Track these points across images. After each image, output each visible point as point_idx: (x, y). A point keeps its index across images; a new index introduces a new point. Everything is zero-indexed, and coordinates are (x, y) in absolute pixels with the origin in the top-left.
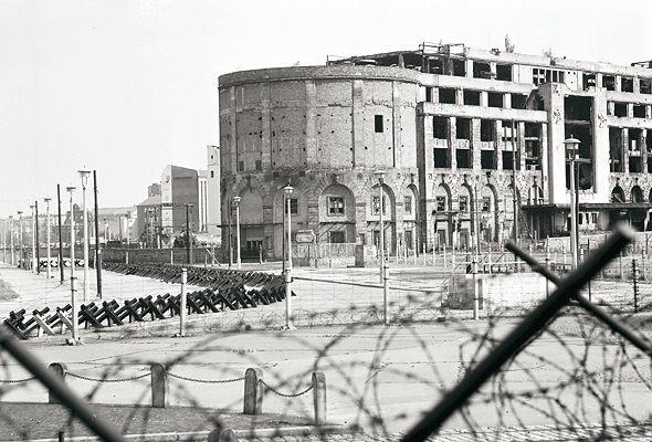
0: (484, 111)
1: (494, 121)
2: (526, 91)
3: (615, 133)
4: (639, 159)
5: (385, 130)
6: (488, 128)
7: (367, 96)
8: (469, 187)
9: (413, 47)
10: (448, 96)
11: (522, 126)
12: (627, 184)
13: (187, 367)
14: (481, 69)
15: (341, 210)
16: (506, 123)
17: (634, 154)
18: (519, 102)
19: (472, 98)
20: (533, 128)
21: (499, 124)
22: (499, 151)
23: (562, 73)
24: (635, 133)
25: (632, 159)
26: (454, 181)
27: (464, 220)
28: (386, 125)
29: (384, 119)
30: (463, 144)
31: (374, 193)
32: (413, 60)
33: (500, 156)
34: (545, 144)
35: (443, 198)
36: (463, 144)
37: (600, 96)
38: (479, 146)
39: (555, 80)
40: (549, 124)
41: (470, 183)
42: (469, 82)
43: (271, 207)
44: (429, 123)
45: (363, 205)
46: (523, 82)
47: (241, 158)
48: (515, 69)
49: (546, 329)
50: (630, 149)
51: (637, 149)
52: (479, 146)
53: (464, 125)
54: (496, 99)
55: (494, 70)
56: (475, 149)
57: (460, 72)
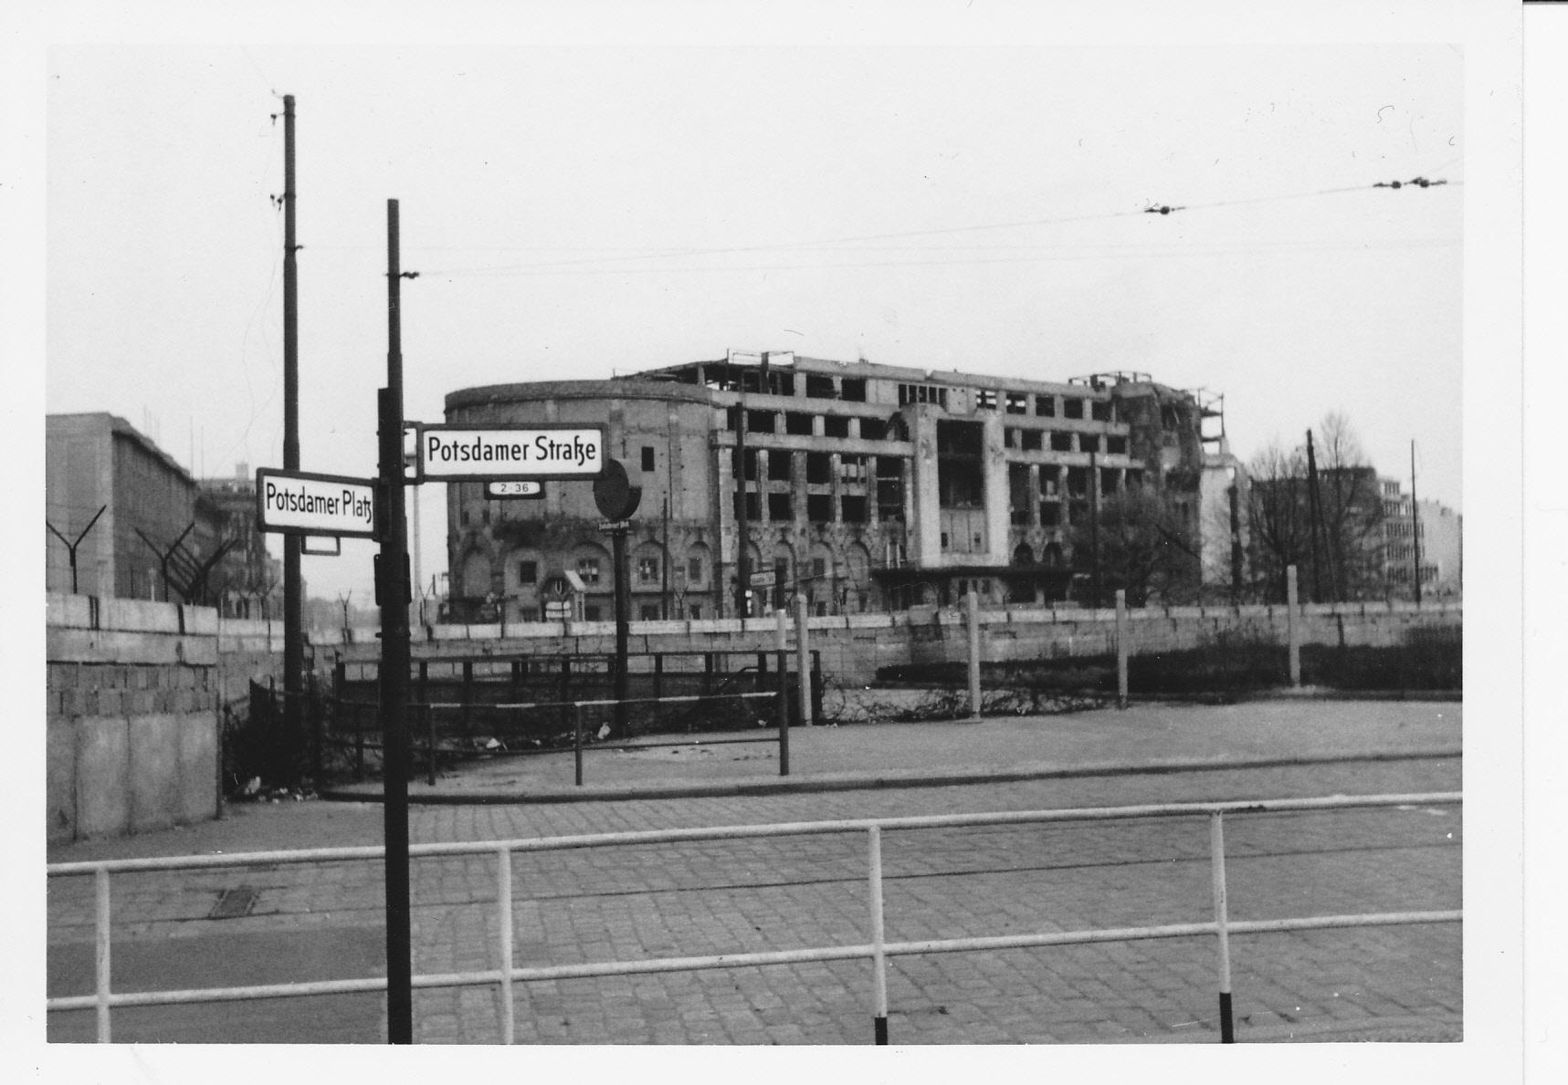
0: (817, 440)
1: (829, 454)
2: (884, 415)
3: (1017, 473)
4: (1056, 506)
5: (657, 467)
6: (818, 465)
7: (630, 420)
8: (790, 546)
9: (715, 356)
10: (763, 421)
11: (873, 462)
12: (1038, 540)
13: (212, 800)
14: (819, 384)
15: (595, 578)
16: (848, 458)
17: (1049, 498)
18: (872, 429)
19: (799, 423)
20: (890, 465)
21: (836, 459)
22: (838, 495)
23: (943, 391)
24: (1049, 471)
25: (1044, 506)
26: (766, 537)
27: (1340, 627)
28: (660, 462)
29: (657, 453)
30: (780, 486)
31: (692, 554)
32: (721, 372)
33: (838, 503)
34: (909, 486)
35: (785, 560)
36: (780, 486)
37: (994, 425)
38: (804, 490)
39: (923, 400)
40: (913, 458)
41: (791, 539)
42: (801, 402)
43: (502, 574)
44: (725, 457)
45: (681, 569)
46: (882, 400)
47: (467, 506)
48: (871, 387)
49: (1342, 646)
50: (1044, 491)
51: (1056, 493)
52: (804, 490)
53: (781, 462)
54: (837, 426)
55: (838, 386)
56: (800, 492)
57: (788, 390)
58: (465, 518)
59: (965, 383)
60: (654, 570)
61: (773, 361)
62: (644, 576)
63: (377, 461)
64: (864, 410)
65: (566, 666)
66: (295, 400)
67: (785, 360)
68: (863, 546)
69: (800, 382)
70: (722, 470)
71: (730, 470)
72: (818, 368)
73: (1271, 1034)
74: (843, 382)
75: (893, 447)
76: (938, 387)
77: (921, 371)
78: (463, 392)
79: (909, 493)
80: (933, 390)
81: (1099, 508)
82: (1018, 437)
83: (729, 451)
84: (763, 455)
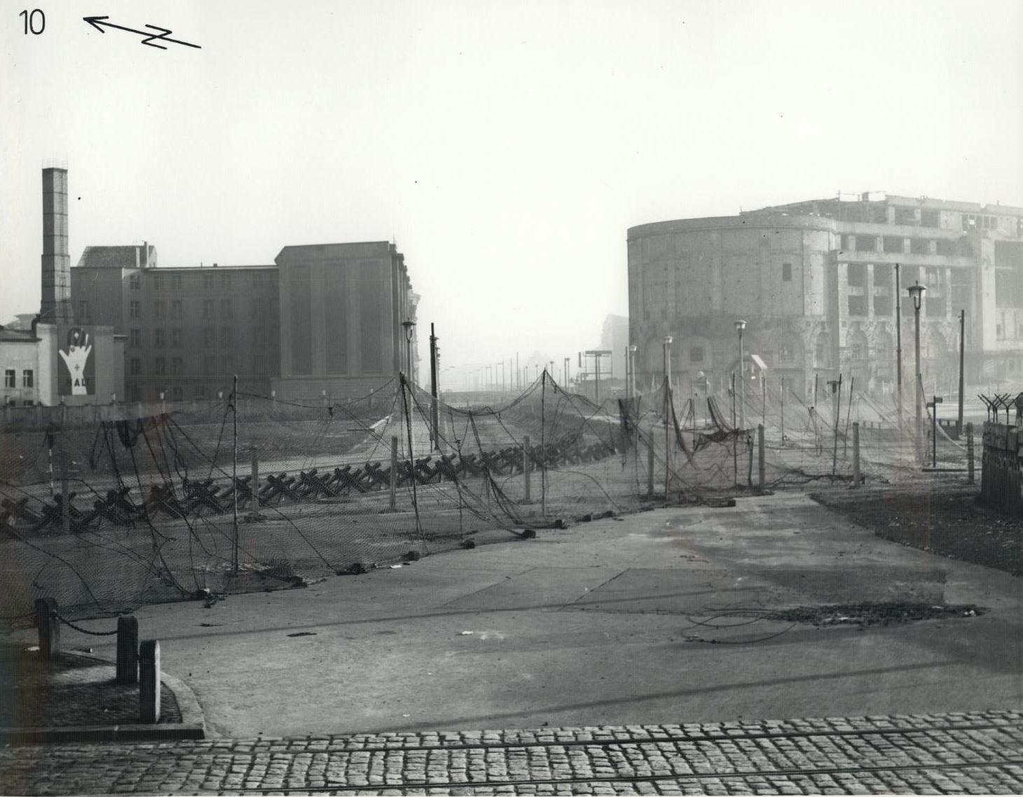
5: (793, 278)
9: (828, 195)
10: (866, 243)
14: (904, 214)
16: (930, 269)
19: (893, 245)
23: (994, 220)
29: (793, 267)
32: (831, 208)
44: (842, 270)
48: (943, 217)
54: (919, 246)
55: (918, 216)
57: (882, 220)
58: (647, 316)
59: (953, 207)
60: (791, 352)
61: (872, 198)
62: (783, 357)
63: (221, 264)
64: (938, 234)
65: (949, 423)
66: (45, 214)
67: (882, 198)
68: (940, 334)
69: (891, 213)
70: (840, 279)
71: (846, 280)
72: (902, 203)
73: (86, 616)
74: (922, 213)
75: (962, 262)
76: (990, 216)
77: (978, 205)
78: (640, 227)
79: (974, 296)
80: (986, 218)
81: (123, 276)
82: (852, 244)
83: (845, 266)
84: (871, 268)
